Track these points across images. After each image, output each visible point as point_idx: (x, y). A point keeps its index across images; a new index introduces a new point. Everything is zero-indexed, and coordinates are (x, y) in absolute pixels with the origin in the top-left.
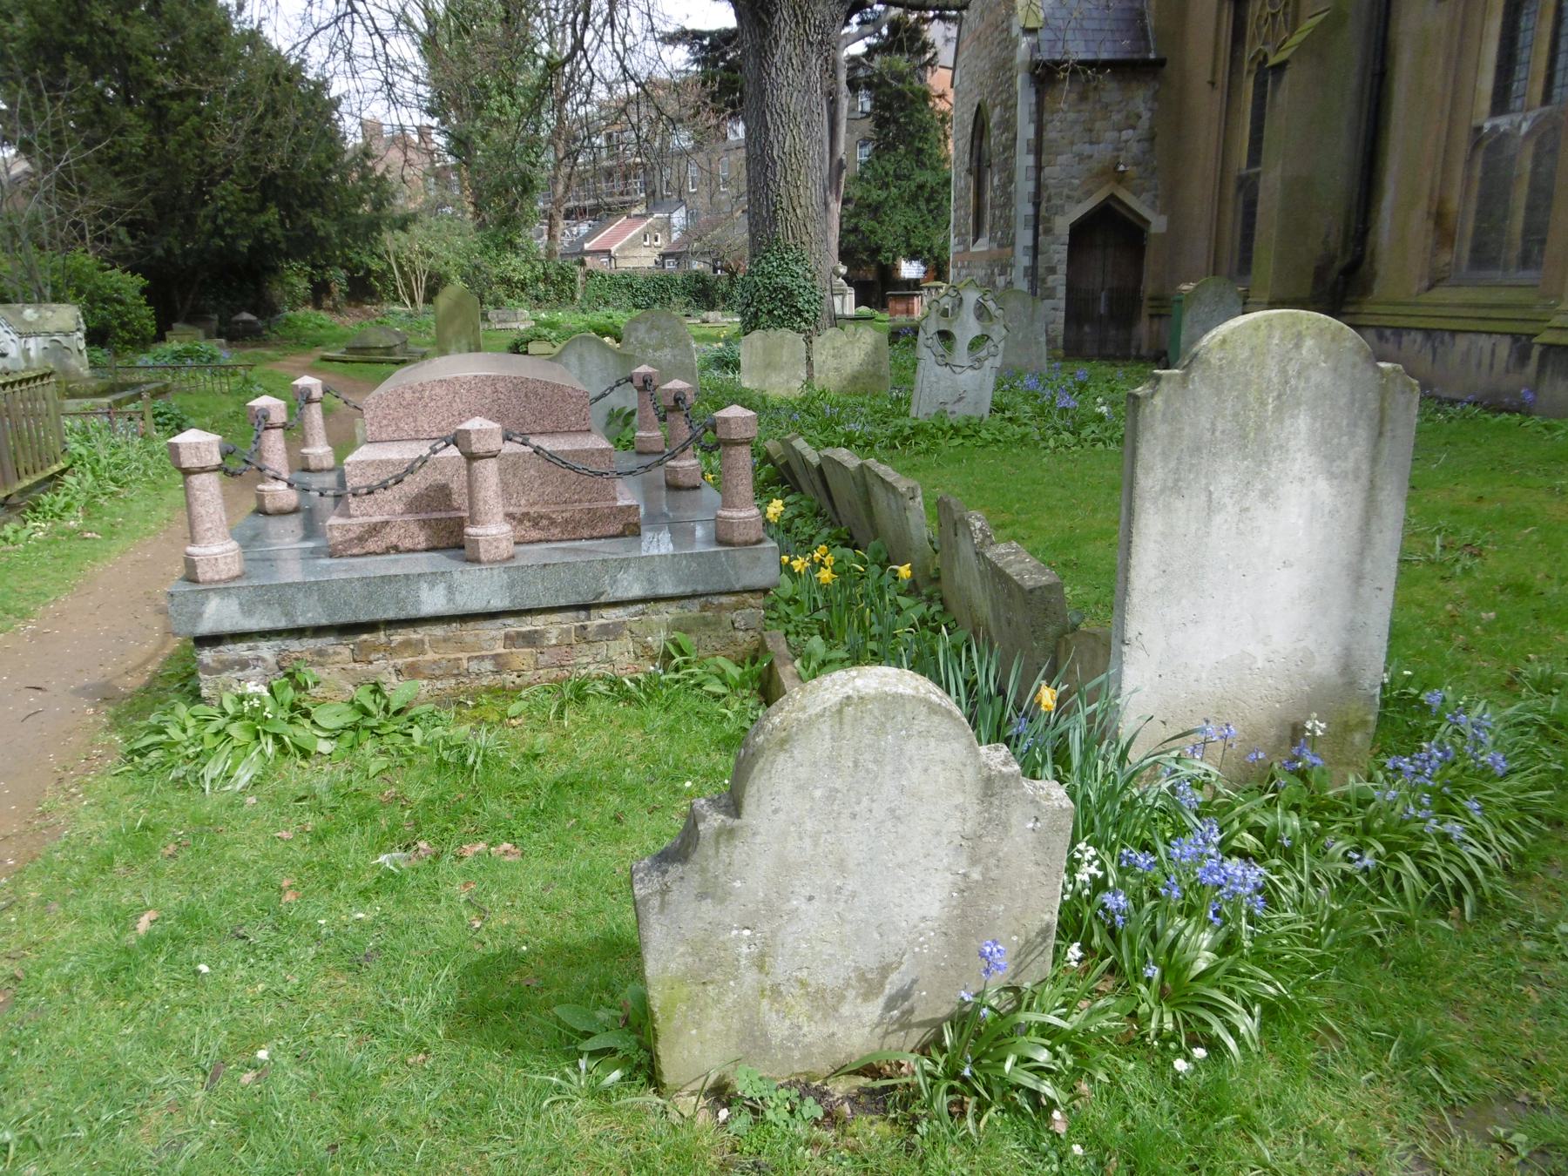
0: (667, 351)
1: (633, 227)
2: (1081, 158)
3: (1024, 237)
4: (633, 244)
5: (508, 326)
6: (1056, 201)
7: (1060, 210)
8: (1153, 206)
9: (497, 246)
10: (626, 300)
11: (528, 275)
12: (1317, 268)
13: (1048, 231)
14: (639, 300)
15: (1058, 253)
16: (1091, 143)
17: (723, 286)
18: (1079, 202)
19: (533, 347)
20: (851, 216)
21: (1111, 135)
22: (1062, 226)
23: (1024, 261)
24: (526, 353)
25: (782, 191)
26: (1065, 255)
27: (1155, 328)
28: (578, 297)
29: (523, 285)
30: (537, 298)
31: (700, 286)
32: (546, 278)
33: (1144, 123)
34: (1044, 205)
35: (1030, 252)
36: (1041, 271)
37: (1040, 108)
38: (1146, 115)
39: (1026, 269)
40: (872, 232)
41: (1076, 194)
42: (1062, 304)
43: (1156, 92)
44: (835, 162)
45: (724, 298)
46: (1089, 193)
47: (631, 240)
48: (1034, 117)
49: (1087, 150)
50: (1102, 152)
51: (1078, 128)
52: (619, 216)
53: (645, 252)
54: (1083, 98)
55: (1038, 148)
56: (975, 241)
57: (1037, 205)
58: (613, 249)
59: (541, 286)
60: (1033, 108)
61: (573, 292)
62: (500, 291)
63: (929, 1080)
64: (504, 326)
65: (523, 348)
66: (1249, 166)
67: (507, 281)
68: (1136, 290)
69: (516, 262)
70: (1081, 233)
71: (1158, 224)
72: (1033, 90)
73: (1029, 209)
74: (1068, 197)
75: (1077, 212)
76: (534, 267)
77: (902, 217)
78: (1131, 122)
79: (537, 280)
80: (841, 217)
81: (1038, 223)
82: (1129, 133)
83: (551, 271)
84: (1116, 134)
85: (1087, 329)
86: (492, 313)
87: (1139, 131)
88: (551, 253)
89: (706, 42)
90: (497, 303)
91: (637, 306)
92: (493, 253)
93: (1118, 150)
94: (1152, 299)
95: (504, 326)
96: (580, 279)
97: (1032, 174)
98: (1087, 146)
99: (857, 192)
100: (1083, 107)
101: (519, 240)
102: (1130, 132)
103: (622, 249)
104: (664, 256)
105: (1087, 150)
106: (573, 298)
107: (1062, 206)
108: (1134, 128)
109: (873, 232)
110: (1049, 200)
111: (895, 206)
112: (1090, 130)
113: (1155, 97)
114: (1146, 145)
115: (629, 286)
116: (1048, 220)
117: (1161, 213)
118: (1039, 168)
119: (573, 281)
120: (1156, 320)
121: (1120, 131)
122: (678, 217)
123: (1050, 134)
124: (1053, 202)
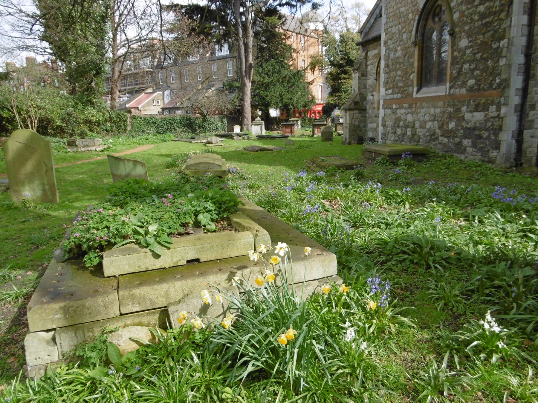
1: (147, 98)
4: (148, 104)
5: (89, 149)
9: (82, 103)
10: (153, 130)
11: (101, 118)
14: (160, 130)
17: (199, 122)
20: (256, 89)
23: (516, 100)
28: (129, 129)
29: (99, 125)
30: (106, 130)
31: (188, 122)
32: (111, 119)
35: (520, 93)
39: (516, 106)
44: (248, 65)
52: (141, 93)
53: (153, 108)
56: (418, 91)
58: (140, 107)
59: (108, 124)
61: (125, 127)
62: (85, 129)
64: (86, 149)
67: (88, 122)
69: (94, 111)
73: (521, 59)
76: (104, 114)
77: (277, 90)
80: (251, 89)
83: (113, 116)
86: (79, 141)
88: (112, 107)
89: (183, 11)
90: (82, 135)
91: (158, 132)
92: (81, 107)
95: (86, 149)
96: (129, 120)
97: (526, 31)
99: (258, 78)
101: (95, 100)
103: (143, 107)
104: (163, 109)
106: (125, 130)
115: (154, 123)
119: (125, 121)
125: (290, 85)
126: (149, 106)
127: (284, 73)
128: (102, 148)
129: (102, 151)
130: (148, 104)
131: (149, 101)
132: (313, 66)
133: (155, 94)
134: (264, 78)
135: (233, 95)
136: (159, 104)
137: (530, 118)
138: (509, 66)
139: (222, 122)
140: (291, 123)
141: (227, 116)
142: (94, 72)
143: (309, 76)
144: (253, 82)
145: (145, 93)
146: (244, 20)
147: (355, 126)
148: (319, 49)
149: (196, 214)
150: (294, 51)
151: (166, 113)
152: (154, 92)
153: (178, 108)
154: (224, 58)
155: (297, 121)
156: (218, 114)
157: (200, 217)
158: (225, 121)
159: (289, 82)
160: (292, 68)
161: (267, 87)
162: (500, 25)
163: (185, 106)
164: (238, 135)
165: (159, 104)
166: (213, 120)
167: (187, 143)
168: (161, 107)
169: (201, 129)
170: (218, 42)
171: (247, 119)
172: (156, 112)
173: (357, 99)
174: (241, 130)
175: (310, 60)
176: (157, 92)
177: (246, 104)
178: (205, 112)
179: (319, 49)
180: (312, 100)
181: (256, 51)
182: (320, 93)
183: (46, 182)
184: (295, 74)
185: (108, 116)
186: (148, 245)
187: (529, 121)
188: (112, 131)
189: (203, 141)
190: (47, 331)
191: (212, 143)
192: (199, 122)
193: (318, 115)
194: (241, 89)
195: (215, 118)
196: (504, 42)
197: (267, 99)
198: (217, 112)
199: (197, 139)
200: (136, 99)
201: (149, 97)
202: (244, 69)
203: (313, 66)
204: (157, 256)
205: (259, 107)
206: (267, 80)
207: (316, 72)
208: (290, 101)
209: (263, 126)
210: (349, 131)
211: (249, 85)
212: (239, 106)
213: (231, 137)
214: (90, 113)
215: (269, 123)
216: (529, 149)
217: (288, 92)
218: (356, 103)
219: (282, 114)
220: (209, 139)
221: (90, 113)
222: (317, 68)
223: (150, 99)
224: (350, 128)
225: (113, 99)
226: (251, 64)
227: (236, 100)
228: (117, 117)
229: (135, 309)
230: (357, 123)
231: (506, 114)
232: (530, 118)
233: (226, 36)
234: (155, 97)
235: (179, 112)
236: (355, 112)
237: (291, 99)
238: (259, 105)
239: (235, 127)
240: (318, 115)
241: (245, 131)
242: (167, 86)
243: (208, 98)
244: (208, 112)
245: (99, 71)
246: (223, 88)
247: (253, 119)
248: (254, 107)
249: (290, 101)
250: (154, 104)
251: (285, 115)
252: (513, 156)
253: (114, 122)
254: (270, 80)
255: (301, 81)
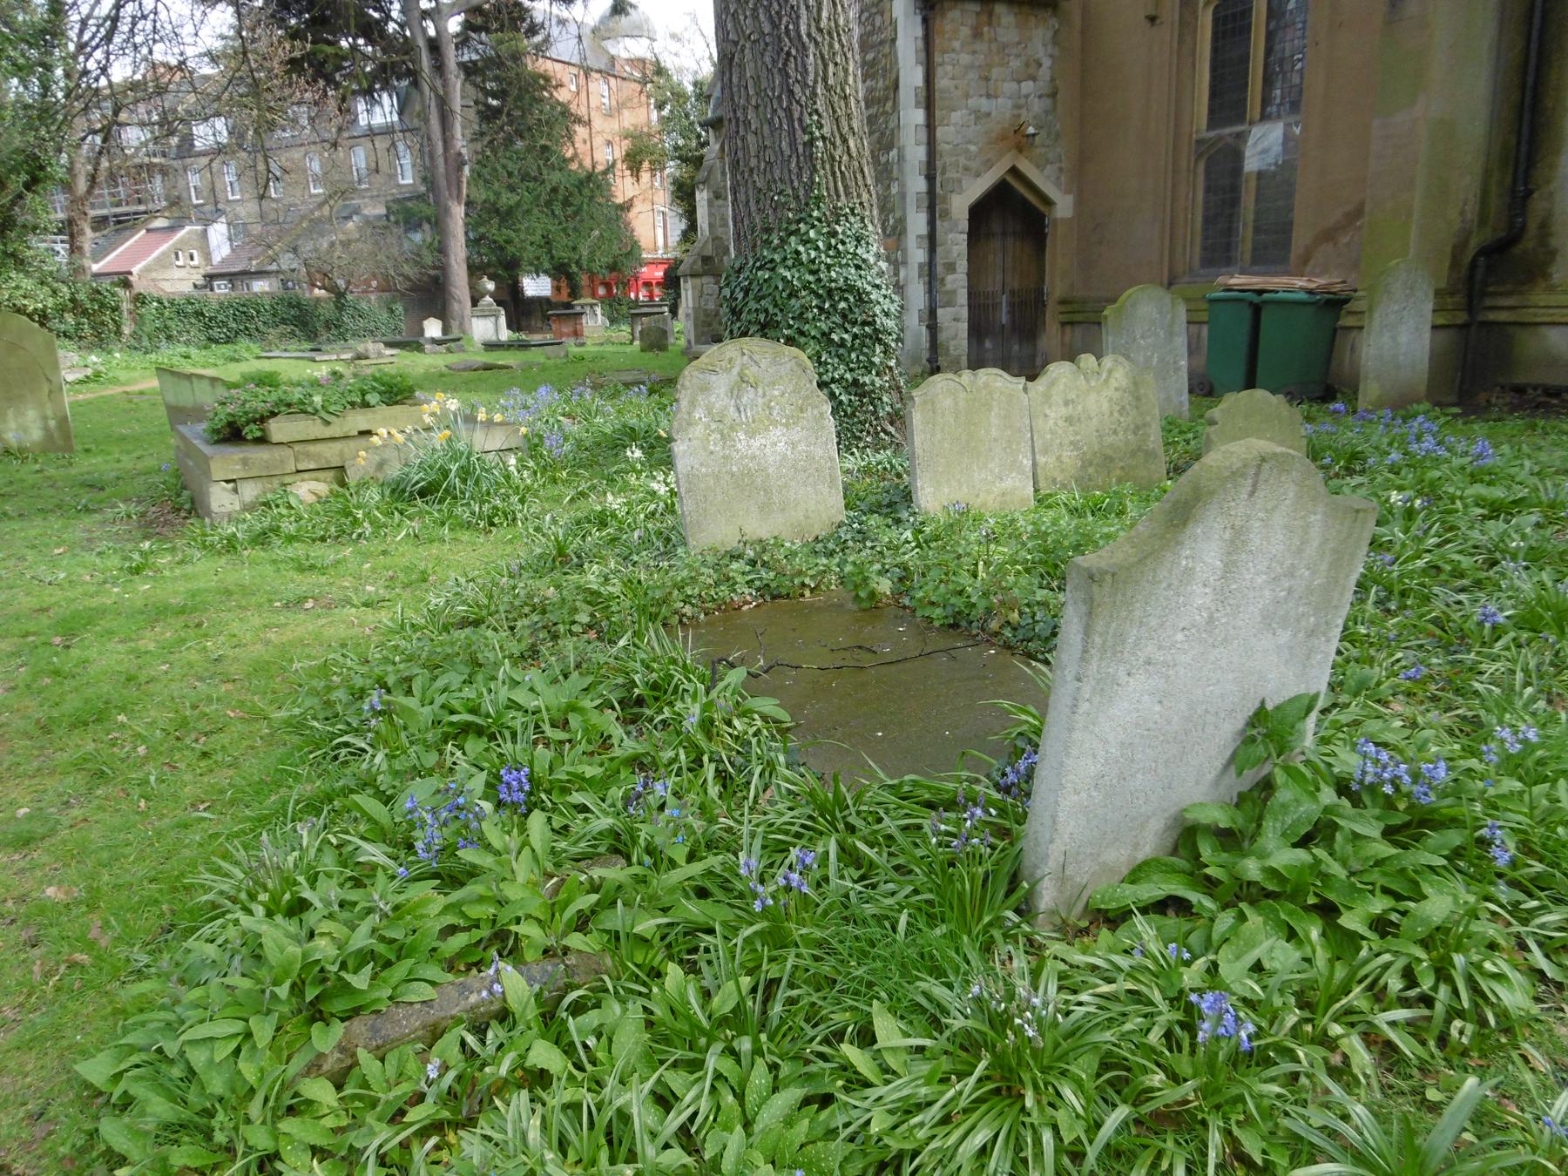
0: (776, 433)
2: (980, 116)
3: (917, 223)
4: (162, 263)
6: (951, 174)
7: (958, 187)
8: (1057, 183)
11: (50, 302)
12: (1454, 247)
13: (946, 214)
14: (215, 333)
15: (956, 243)
16: (989, 96)
18: (978, 175)
19: (279, 429)
21: (1009, 87)
22: (960, 205)
24: (263, 440)
25: (820, 106)
26: (964, 247)
27: (1067, 338)
28: (126, 330)
33: (1045, 73)
34: (938, 179)
35: (925, 244)
36: (939, 269)
37: (928, 39)
38: (1047, 63)
39: (921, 266)
40: (507, 242)
41: (974, 165)
42: (964, 313)
43: (1056, 32)
45: (328, 325)
46: (989, 165)
47: (158, 259)
48: (923, 55)
49: (984, 104)
50: (1001, 108)
51: (972, 75)
52: (134, 229)
53: (178, 274)
54: (977, 34)
55: (929, 101)
57: (930, 178)
60: (920, 44)
61: (118, 325)
63: (569, 1112)
65: (252, 431)
66: (1213, 122)
68: (1040, 292)
69: (28, 284)
70: (979, 213)
71: (1063, 206)
72: (919, 19)
74: (966, 169)
75: (976, 188)
78: (1031, 71)
79: (61, 310)
80: (466, 225)
81: (933, 205)
82: (1028, 86)
83: (82, 296)
84: (1014, 85)
85: (988, 344)
87: (1041, 84)
91: (210, 339)
93: (1018, 107)
94: (1063, 302)
97: (923, 136)
98: (983, 100)
99: (481, 195)
100: (978, 46)
102: (1031, 83)
103: (147, 269)
105: (984, 104)
106: (118, 332)
107: (960, 181)
108: (1034, 79)
109: (509, 242)
110: (943, 173)
111: (528, 211)
112: (987, 79)
113: (1055, 40)
114: (1048, 102)
116: (945, 199)
117: (1067, 192)
118: (930, 126)
120: (1068, 329)
121: (1019, 82)
122: (218, 233)
123: (942, 83)
124: (948, 175)
125: (570, 210)
126: (164, 267)
127: (555, 177)
128: (80, 376)
129: (81, 382)
130: (162, 263)
131: (163, 253)
132: (634, 161)
133: (181, 234)
134: (498, 194)
135: (417, 237)
136: (196, 262)
137: (949, 287)
138: (903, 195)
139: (392, 311)
140: (578, 309)
141: (403, 295)
142: (24, 177)
143: (624, 187)
144: (469, 204)
145: (148, 231)
146: (432, 32)
147: (706, 313)
148: (644, 116)
149: (364, 393)
150: (579, 120)
151: (221, 289)
152: (172, 229)
153: (260, 274)
154: (388, 131)
155: (592, 306)
156: (380, 289)
157: (368, 397)
158: (399, 308)
159: (566, 203)
160: (574, 166)
161: (506, 216)
162: (887, 122)
163: (284, 267)
164: (434, 341)
165: (196, 262)
166: (364, 305)
167: (301, 362)
168: (202, 271)
169: (334, 331)
170: (368, 93)
171: (460, 302)
172: (187, 288)
173: (709, 251)
174: (445, 330)
175: (626, 144)
176: (188, 228)
177: (453, 262)
178: (341, 283)
179: (644, 116)
180: (630, 253)
181: (472, 114)
182: (660, 232)
183: (49, 413)
184: (581, 182)
185: (68, 297)
186: (316, 412)
187: (947, 292)
188: (81, 338)
189: (344, 357)
190: (227, 482)
191: (367, 358)
192: (327, 311)
193: (657, 291)
194: (438, 223)
195: (369, 301)
196: (894, 153)
197: (510, 249)
198: (374, 283)
199: (328, 353)
200: (127, 244)
201: (165, 241)
202: (441, 168)
203: (634, 161)
204: (328, 423)
205: (491, 270)
206: (507, 199)
207: (645, 176)
208: (572, 255)
209: (503, 320)
210: (696, 326)
211: (458, 211)
212: (435, 267)
213: (419, 348)
214: (17, 287)
215: (520, 311)
216: (952, 343)
217: (564, 230)
218: (706, 260)
219: (557, 289)
220: (361, 348)
221: (17, 287)
222: (646, 165)
223: (164, 247)
224: (696, 319)
225: (75, 249)
226: (460, 154)
227: (425, 252)
228: (92, 300)
229: (312, 466)
230: (711, 306)
231: (906, 278)
232: (949, 287)
233: (384, 76)
234: (181, 240)
235: (260, 286)
236: (705, 279)
237: (574, 249)
238: (489, 265)
239: (426, 323)
240: (657, 291)
241: (455, 333)
242: (218, 210)
243: (346, 244)
244: (348, 283)
245: (41, 174)
246: (387, 217)
247: (475, 302)
248: (475, 270)
249: (572, 255)
250: (180, 263)
251: (565, 291)
252: (926, 355)
253: (85, 313)
254: (514, 198)
255: (600, 200)
